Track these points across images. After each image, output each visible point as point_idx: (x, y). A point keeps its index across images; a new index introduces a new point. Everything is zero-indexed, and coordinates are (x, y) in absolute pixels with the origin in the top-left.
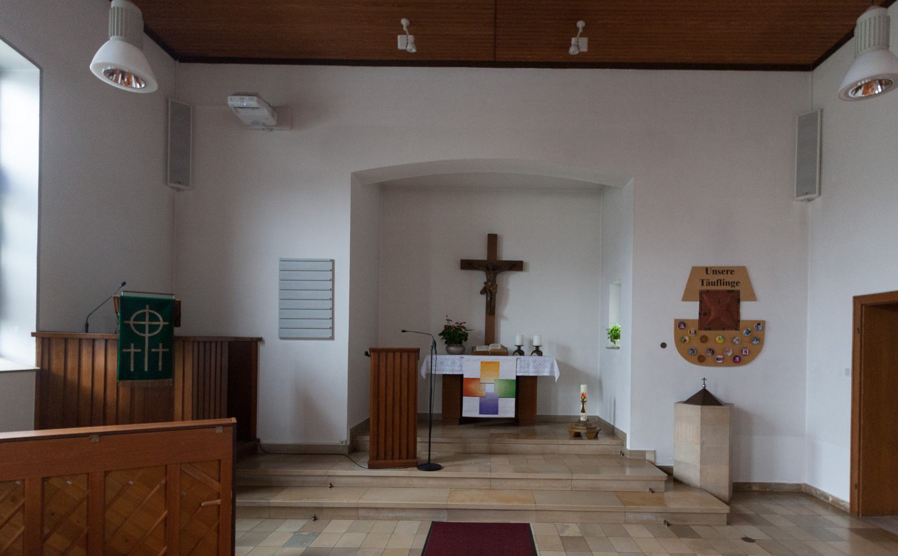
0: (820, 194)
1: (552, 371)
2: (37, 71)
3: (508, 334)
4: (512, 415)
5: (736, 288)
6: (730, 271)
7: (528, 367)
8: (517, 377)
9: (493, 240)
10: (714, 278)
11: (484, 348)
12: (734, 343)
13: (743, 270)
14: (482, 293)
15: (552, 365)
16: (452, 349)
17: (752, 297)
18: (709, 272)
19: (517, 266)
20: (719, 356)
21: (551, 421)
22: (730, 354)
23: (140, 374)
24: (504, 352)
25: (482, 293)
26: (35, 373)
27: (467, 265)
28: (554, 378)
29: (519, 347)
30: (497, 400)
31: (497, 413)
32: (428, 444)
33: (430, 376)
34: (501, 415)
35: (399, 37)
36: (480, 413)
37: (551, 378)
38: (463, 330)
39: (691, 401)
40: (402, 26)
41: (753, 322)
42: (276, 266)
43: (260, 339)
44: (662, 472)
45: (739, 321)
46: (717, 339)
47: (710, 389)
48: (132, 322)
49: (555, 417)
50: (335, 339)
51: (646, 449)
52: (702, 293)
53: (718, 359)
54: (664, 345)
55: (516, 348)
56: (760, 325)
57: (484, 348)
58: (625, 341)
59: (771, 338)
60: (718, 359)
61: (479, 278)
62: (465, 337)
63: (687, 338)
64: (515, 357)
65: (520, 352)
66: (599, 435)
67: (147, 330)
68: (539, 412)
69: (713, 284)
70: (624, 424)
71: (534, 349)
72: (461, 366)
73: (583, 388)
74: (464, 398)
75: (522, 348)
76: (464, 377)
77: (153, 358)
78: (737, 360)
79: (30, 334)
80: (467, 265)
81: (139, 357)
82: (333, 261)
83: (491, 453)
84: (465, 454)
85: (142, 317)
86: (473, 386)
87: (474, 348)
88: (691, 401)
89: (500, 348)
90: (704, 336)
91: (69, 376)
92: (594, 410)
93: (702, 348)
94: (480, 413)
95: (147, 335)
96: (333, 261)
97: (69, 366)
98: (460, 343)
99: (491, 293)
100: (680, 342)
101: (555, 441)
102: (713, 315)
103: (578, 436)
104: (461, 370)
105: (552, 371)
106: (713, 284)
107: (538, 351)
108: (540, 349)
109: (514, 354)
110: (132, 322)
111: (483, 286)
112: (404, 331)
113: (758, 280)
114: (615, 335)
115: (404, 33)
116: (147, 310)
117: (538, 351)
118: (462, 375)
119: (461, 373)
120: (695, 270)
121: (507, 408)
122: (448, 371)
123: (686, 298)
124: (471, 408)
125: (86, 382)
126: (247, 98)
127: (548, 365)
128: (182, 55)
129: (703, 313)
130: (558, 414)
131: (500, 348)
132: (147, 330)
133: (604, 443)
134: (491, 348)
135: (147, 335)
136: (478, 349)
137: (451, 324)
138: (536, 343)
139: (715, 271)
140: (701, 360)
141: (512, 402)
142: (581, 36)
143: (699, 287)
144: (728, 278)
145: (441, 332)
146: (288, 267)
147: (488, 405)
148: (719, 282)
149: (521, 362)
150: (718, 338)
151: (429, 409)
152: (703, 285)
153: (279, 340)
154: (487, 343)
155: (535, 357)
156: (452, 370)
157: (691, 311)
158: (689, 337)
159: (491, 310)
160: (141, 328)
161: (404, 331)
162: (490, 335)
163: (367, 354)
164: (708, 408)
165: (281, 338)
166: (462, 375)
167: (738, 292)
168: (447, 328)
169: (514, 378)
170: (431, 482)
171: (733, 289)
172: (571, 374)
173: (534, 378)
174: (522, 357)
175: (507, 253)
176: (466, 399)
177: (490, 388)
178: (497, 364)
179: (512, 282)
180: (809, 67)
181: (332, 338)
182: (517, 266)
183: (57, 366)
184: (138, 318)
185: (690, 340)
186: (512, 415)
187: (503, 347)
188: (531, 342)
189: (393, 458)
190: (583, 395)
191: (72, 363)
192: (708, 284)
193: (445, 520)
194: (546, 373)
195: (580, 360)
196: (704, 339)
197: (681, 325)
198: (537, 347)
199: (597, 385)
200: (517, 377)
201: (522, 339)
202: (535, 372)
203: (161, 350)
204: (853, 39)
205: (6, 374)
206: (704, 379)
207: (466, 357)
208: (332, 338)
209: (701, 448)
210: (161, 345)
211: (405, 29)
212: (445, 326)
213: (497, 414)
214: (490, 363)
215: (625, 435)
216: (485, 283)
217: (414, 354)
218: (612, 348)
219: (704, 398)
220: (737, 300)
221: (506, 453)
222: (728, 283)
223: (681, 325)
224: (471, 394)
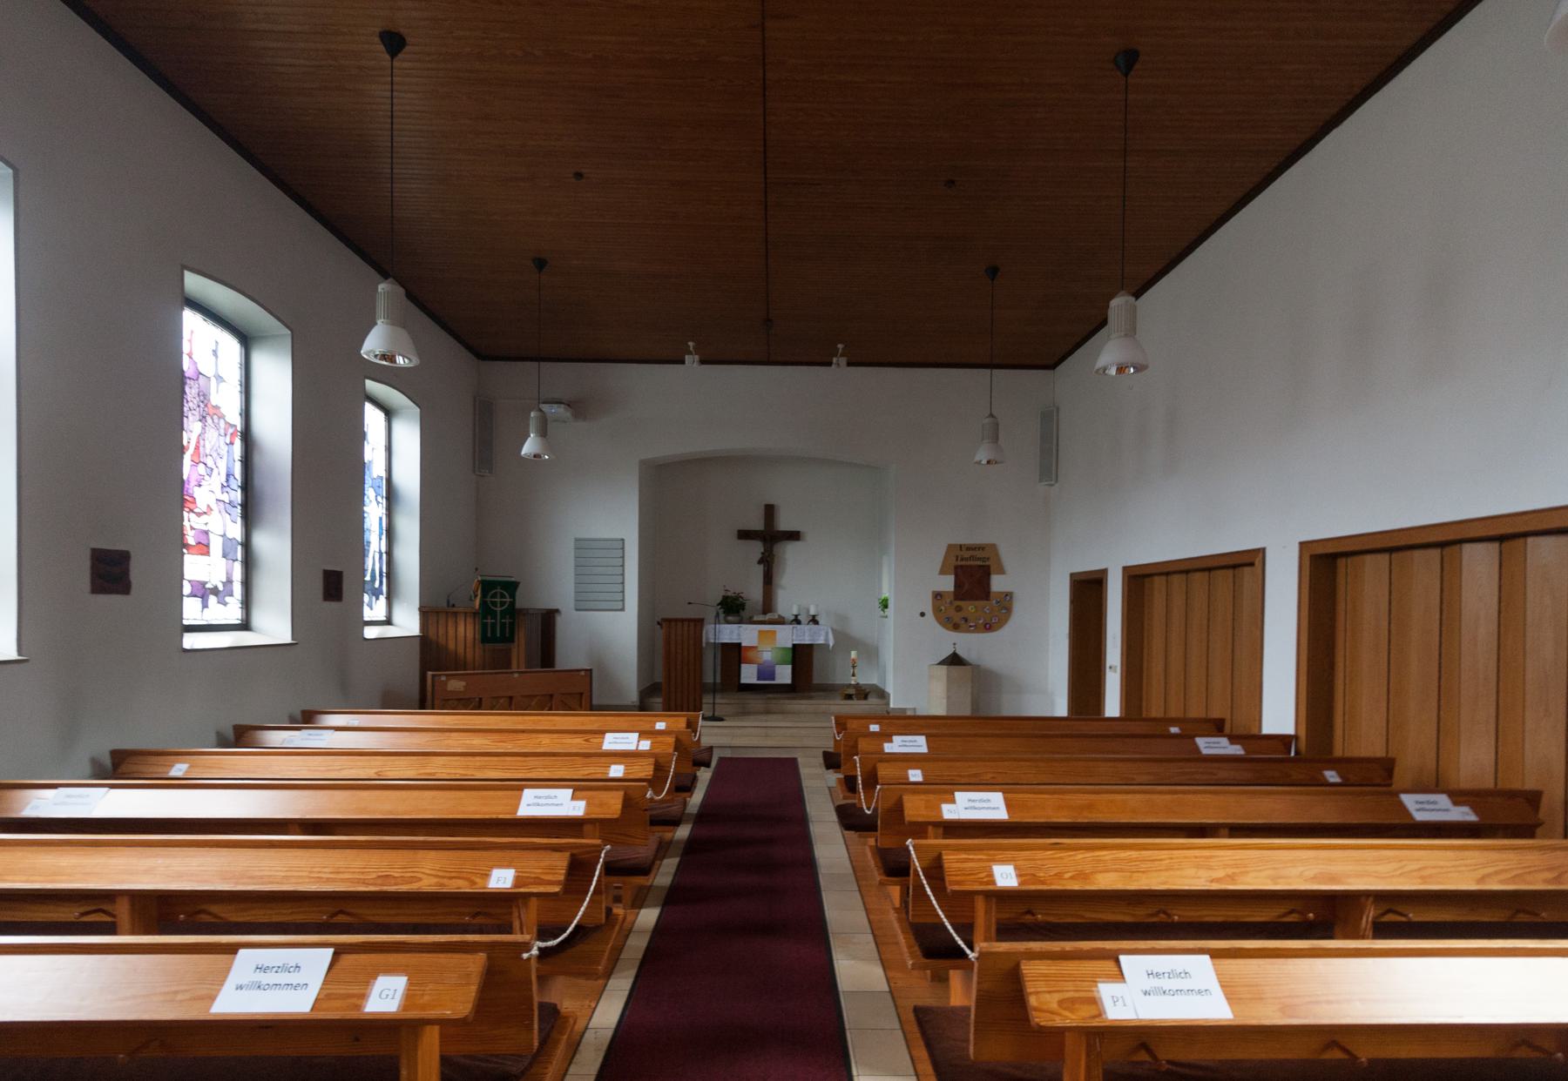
0: (1057, 481)
1: (827, 640)
2: (418, 410)
3: (786, 603)
4: (788, 681)
5: (987, 563)
6: (981, 548)
7: (804, 635)
8: (794, 645)
9: (770, 511)
10: (967, 554)
11: (761, 618)
12: (986, 613)
13: (993, 547)
14: (760, 562)
15: (827, 633)
16: (730, 618)
17: (1001, 571)
18: (963, 549)
19: (794, 536)
20: (972, 624)
21: (828, 690)
22: (981, 622)
23: (493, 640)
24: (781, 621)
25: (760, 562)
26: (419, 638)
27: (744, 535)
28: (829, 645)
29: (796, 616)
30: (774, 667)
31: (774, 679)
32: (712, 706)
33: (707, 643)
34: (778, 681)
35: (687, 357)
36: (758, 679)
37: (825, 646)
38: (741, 600)
39: (942, 663)
40: (689, 347)
41: (1002, 593)
42: (572, 545)
43: (557, 611)
44: (249, 301)
45: (989, 592)
46: (970, 609)
47: (959, 652)
48: (488, 599)
49: (833, 685)
50: (626, 610)
51: (908, 707)
52: (956, 568)
53: (971, 626)
54: (923, 614)
55: (793, 618)
56: (1008, 596)
57: (761, 618)
58: (890, 611)
59: (1018, 607)
60: (971, 626)
61: (757, 548)
62: (742, 606)
63: (943, 608)
64: (791, 626)
65: (797, 621)
66: (869, 696)
67: (499, 605)
68: (816, 680)
69: (966, 559)
70: (890, 689)
71: (811, 618)
72: (739, 635)
73: (853, 654)
74: (743, 666)
75: (799, 617)
76: (743, 645)
77: (503, 625)
78: (988, 627)
79: (111, 602)
80: (744, 535)
81: (494, 626)
82: (623, 540)
83: (768, 712)
84: (744, 713)
85: (494, 596)
86: (750, 654)
87: (751, 618)
88: (942, 663)
89: (777, 617)
90: (957, 606)
91: (440, 640)
92: (865, 678)
93: (957, 617)
94: (758, 679)
95: (499, 609)
96: (623, 540)
97: (440, 634)
98: (738, 612)
99: (768, 565)
100: (937, 611)
101: (827, 702)
102: (966, 586)
103: (849, 697)
104: (739, 639)
105: (827, 640)
106: (966, 559)
107: (814, 621)
108: (817, 618)
109: (791, 623)
110: (488, 599)
111: (760, 556)
112: (690, 603)
113: (1007, 556)
114: (885, 605)
115: (690, 353)
116: (499, 590)
117: (814, 621)
118: (740, 644)
119: (739, 642)
120: (950, 547)
121: (784, 675)
122: (726, 640)
123: (942, 572)
124: (749, 675)
125: (451, 646)
126: (556, 406)
127: (823, 633)
128: (482, 354)
129: (958, 585)
130: (838, 682)
131: (777, 617)
132: (499, 605)
133: (873, 702)
134: (768, 617)
135: (499, 609)
136: (755, 619)
137: (729, 594)
138: (812, 612)
139: (969, 548)
140: (956, 627)
141: (788, 669)
142: (842, 355)
143: (953, 562)
144: (978, 554)
145: (719, 601)
146: (581, 545)
147: (766, 672)
148: (972, 558)
149: (797, 630)
150: (970, 607)
151: (712, 677)
152: (957, 560)
153: (575, 612)
154: (765, 613)
155: (812, 626)
156: (731, 639)
157: (947, 584)
158: (945, 607)
159: (769, 580)
160: (494, 604)
161: (690, 603)
162: (768, 605)
163: (659, 623)
164: (953, 668)
165: (577, 610)
166: (740, 644)
167: (989, 567)
168: (725, 598)
169: (790, 646)
170: (716, 730)
171: (984, 564)
172: (845, 640)
173: (810, 646)
174: (799, 626)
175: (784, 523)
176: (744, 667)
177: (767, 656)
178: (774, 632)
179: (790, 554)
180: (1053, 366)
181: (623, 609)
182: (794, 536)
183: (432, 633)
184: (493, 597)
185: (946, 609)
186: (788, 681)
187: (779, 616)
188: (808, 611)
189: (522, 933)
190: (853, 660)
191: (441, 631)
192: (962, 560)
193: (729, 756)
194: (821, 641)
195: (859, 627)
196: (959, 609)
197: (938, 596)
198: (814, 616)
199: (871, 653)
200: (794, 645)
201: (799, 609)
202: (810, 640)
203: (507, 621)
204: (1106, 327)
205: (269, 648)
206: (955, 644)
207: (744, 626)
208: (623, 609)
209: (947, 702)
210: (508, 617)
211: (691, 349)
212: (724, 596)
213: (774, 679)
214: (768, 631)
215: (889, 695)
216: (763, 553)
217: (699, 623)
218: (883, 617)
219: (954, 660)
220: (988, 575)
221: (782, 713)
222: (979, 559)
223: (938, 596)
224: (750, 662)
